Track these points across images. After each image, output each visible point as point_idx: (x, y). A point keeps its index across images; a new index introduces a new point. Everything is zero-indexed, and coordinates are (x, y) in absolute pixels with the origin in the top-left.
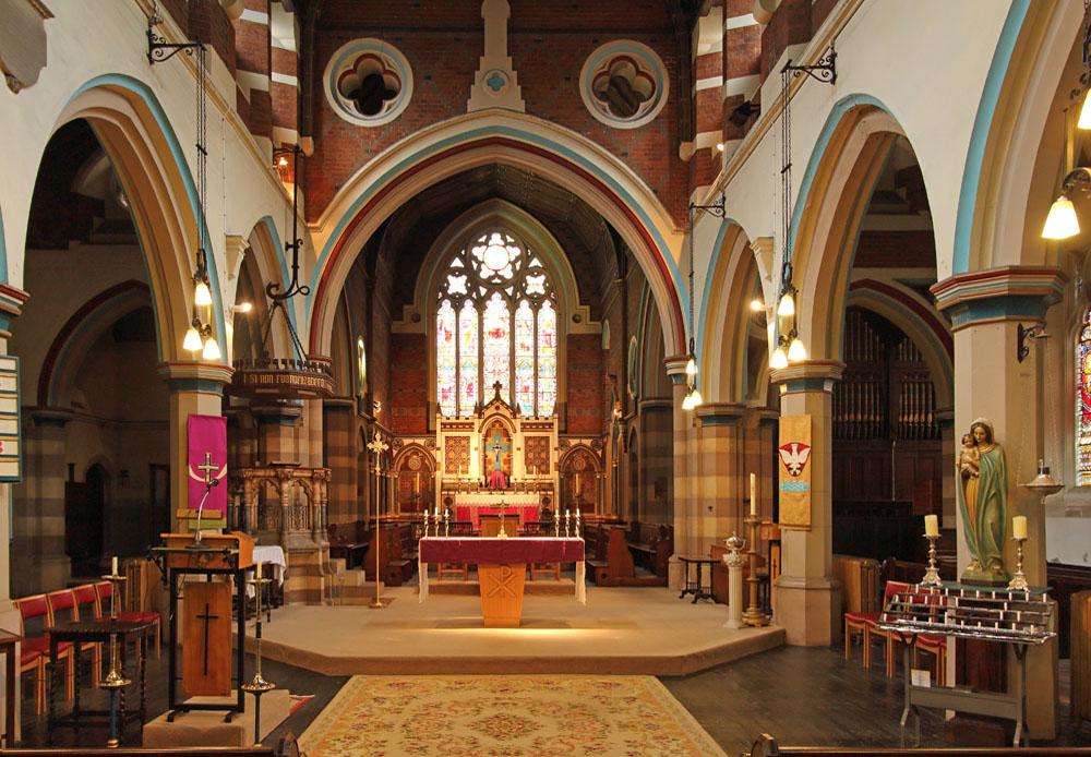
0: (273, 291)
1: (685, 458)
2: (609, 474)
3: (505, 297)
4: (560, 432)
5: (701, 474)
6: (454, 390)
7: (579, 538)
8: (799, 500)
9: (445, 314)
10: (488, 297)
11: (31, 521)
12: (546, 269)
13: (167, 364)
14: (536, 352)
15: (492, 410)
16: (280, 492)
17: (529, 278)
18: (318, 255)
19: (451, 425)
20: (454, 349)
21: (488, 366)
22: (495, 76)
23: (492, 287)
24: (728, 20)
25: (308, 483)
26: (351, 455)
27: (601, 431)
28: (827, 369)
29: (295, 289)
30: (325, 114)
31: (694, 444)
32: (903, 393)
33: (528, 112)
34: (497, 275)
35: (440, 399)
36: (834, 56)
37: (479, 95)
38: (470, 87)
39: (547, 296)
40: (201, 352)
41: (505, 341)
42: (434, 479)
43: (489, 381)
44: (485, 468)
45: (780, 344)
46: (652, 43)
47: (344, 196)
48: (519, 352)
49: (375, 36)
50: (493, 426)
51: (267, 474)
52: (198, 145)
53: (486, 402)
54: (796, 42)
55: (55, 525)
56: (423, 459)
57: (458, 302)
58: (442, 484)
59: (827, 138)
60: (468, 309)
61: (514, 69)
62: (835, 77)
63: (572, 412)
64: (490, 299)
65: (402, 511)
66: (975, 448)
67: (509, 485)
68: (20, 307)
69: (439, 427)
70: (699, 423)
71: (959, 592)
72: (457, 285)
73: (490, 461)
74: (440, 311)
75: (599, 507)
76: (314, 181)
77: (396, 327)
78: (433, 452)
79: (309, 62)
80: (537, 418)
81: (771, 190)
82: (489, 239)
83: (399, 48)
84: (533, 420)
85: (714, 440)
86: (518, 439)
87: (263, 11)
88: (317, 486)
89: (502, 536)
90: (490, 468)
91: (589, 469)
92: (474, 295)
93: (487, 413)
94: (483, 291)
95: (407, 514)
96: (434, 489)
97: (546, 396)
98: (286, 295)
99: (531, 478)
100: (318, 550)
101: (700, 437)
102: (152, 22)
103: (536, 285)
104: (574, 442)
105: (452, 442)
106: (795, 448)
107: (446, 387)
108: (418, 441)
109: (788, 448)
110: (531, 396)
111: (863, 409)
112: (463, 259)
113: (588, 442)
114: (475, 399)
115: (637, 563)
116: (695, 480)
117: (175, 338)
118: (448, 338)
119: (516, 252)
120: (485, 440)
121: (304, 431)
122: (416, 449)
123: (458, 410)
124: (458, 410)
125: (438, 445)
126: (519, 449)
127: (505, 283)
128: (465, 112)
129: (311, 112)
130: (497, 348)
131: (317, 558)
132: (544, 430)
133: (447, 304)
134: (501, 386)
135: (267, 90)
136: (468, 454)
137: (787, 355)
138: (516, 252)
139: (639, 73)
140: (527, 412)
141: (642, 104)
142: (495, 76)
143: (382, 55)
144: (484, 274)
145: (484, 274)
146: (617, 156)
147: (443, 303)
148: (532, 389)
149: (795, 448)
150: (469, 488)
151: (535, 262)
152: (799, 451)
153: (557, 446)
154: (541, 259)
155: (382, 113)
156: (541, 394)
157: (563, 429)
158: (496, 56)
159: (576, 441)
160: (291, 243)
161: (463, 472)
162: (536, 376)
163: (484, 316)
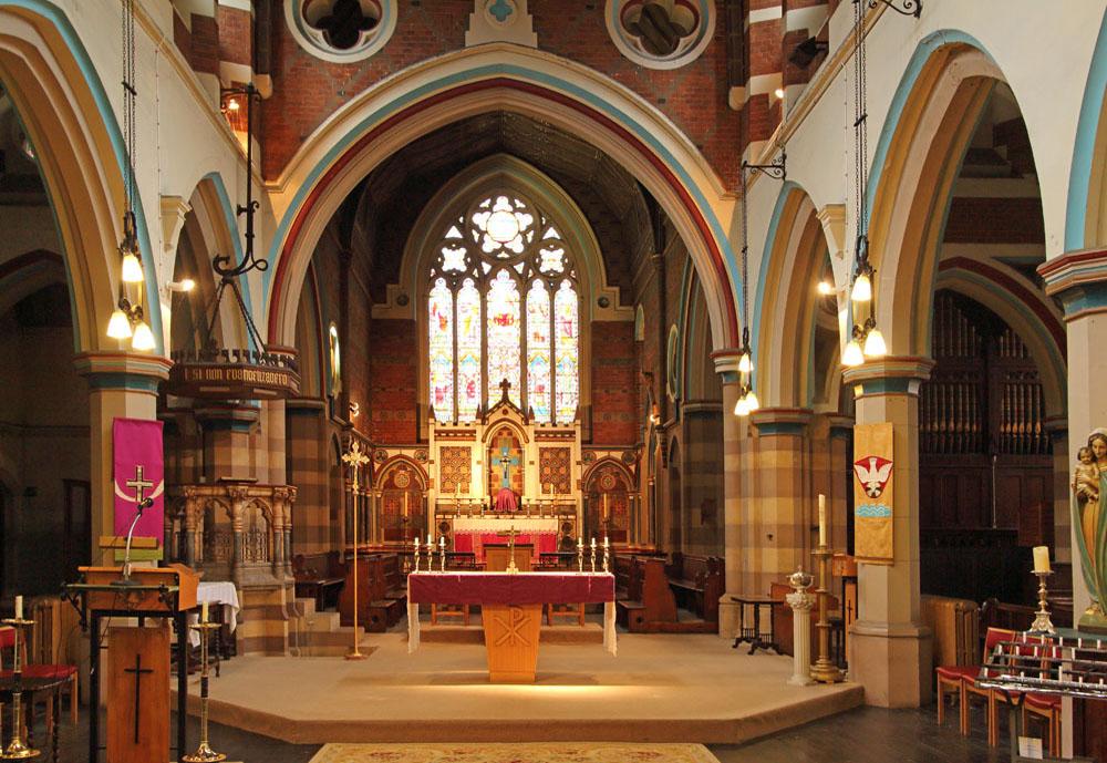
0: (222, 266)
1: (738, 475)
2: (644, 494)
3: (514, 274)
4: (583, 442)
5: (758, 494)
7: (607, 574)
8: (878, 528)
9: (440, 295)
10: (492, 274)
12: (565, 242)
13: (85, 356)
16: (231, 515)
17: (543, 252)
18: (279, 220)
19: (447, 432)
21: (493, 360)
23: (497, 263)
25: (268, 504)
26: (321, 470)
28: (912, 367)
29: (250, 263)
31: (749, 458)
32: (1005, 397)
33: (541, 47)
34: (503, 249)
35: (433, 400)
36: (784, 157)
37: (480, 28)
39: (566, 275)
41: (514, 330)
43: (495, 379)
44: (490, 486)
45: (854, 335)
48: (531, 343)
50: (500, 434)
51: (215, 492)
52: (124, 83)
53: (491, 405)
56: (412, 474)
57: (455, 280)
58: (437, 505)
60: (469, 290)
63: (598, 418)
65: (386, 539)
66: (1094, 465)
67: (520, 507)
70: (756, 432)
71: (1076, 641)
74: (433, 292)
76: (272, 129)
77: (378, 311)
78: (425, 466)
80: (554, 425)
82: (493, 203)
84: (549, 428)
86: (531, 451)
88: (279, 507)
89: (512, 571)
90: (496, 486)
91: (620, 488)
92: (475, 272)
93: (493, 418)
94: (487, 268)
95: (394, 543)
96: (426, 513)
97: (566, 398)
98: (238, 271)
99: (547, 499)
100: (280, 587)
101: (757, 449)
103: (552, 260)
104: (600, 455)
105: (448, 454)
106: (873, 463)
107: (441, 386)
108: (406, 452)
110: (547, 398)
112: (462, 228)
113: (618, 455)
114: (477, 401)
116: (750, 502)
117: (96, 322)
118: (442, 326)
119: (527, 220)
120: (490, 452)
121: (262, 439)
122: (403, 463)
123: (456, 414)
124: (456, 414)
126: (532, 463)
127: (509, 263)
130: (504, 339)
131: (280, 599)
132: (563, 439)
133: (441, 283)
134: (509, 385)
135: (212, 15)
136: (469, 467)
137: (862, 348)
138: (527, 220)
140: (542, 417)
144: (488, 247)
145: (488, 247)
146: (651, 102)
147: (437, 282)
148: (548, 389)
149: (873, 463)
150: (471, 511)
151: (551, 233)
152: (878, 466)
153: (579, 459)
155: (359, 46)
156: (559, 394)
157: (587, 438)
160: (244, 206)
161: (463, 491)
163: (488, 298)
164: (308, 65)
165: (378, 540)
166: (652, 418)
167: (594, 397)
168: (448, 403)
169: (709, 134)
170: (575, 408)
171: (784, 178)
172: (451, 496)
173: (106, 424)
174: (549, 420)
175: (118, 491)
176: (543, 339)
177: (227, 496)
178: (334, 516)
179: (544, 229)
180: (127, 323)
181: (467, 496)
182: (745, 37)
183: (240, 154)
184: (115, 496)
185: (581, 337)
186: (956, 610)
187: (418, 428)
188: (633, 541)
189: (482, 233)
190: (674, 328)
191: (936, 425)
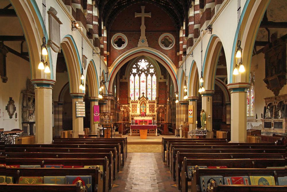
0: (103, 82)
1: (178, 111)
2: (167, 113)
3: (145, 73)
4: (157, 103)
5: (180, 114)
6: (134, 94)
7: (156, 125)
8: (191, 119)
9: (132, 77)
10: (141, 73)
11: (57, 122)
12: (154, 67)
13: (90, 97)
14: (152, 86)
15: (142, 99)
16: (105, 117)
17: (150, 69)
18: (110, 73)
19: (133, 102)
20: (134, 85)
21: (141, 89)
22: (143, 40)
23: (142, 72)
24: (195, 12)
26: (113, 110)
27: (166, 103)
30: (111, 47)
31: (179, 108)
33: (149, 47)
34: (143, 69)
35: (130, 96)
37: (140, 44)
38: (138, 42)
40: (44, 70)
41: (145, 83)
42: (129, 114)
43: (141, 92)
45: (236, 67)
46: (172, 34)
47: (115, 62)
48: (148, 86)
49: (121, 33)
52: (43, 4)
53: (141, 97)
54: (190, 46)
55: (61, 123)
56: (127, 109)
57: (134, 75)
59: (193, 64)
61: (146, 39)
62: (212, 33)
63: (160, 99)
64: (142, 74)
67: (146, 115)
68: (54, 83)
69: (130, 102)
70: (180, 104)
72: (134, 71)
73: (142, 110)
74: (131, 77)
75: (165, 120)
76: (110, 60)
77: (121, 80)
78: (129, 108)
79: (109, 38)
80: (152, 100)
81: (198, 56)
82: (141, 60)
83: (125, 35)
84: (151, 101)
85: (183, 108)
86: (148, 105)
87: (91, 11)
88: (111, 116)
89: (144, 125)
90: (141, 111)
91: (163, 112)
92: (138, 73)
93: (141, 99)
94: (140, 72)
97: (154, 95)
98: (105, 82)
101: (180, 107)
102: (93, 50)
103: (152, 71)
104: (160, 106)
105: (133, 106)
106: (191, 110)
107: (132, 94)
108: (126, 106)
109: (190, 110)
110: (151, 96)
111: (218, 100)
112: (136, 65)
113: (163, 106)
114: (138, 96)
115: (169, 131)
116: (179, 115)
117: (35, 65)
118: (132, 83)
119: (148, 63)
120: (140, 105)
121: (107, 106)
122: (125, 108)
123: (135, 99)
124: (135, 99)
125: (130, 106)
127: (145, 70)
128: (137, 47)
129: (109, 47)
130: (143, 85)
133: (132, 75)
134: (144, 93)
135: (80, 8)
136: (137, 108)
137: (238, 70)
138: (148, 63)
139: (169, 39)
140: (150, 99)
141: (170, 45)
142: (143, 40)
143: (122, 36)
144: (140, 68)
145: (140, 68)
146: (165, 55)
147: (131, 75)
148: (151, 94)
149: (191, 110)
151: (152, 66)
152: (191, 111)
154: (153, 65)
155: (122, 47)
156: (153, 95)
157: (158, 103)
158: (143, 36)
159: (160, 106)
160: (106, 73)
161: (136, 112)
162: (152, 91)
163: (140, 78)
164: (114, 50)
165: (121, 121)
166: (168, 100)
167: (159, 96)
168: (133, 97)
169: (174, 59)
170: (155, 97)
171: (211, 33)
172: (134, 113)
173: (93, 106)
174: (151, 99)
175: (94, 115)
176: (150, 85)
177: (104, 115)
178: (115, 117)
179: (150, 65)
180: (43, 65)
181: (136, 113)
182: (179, 45)
183: (106, 65)
184: (94, 115)
185: (157, 84)
186: (256, 139)
187: (128, 101)
188: (165, 121)
189: (139, 66)
190: (171, 85)
191: (214, 102)
